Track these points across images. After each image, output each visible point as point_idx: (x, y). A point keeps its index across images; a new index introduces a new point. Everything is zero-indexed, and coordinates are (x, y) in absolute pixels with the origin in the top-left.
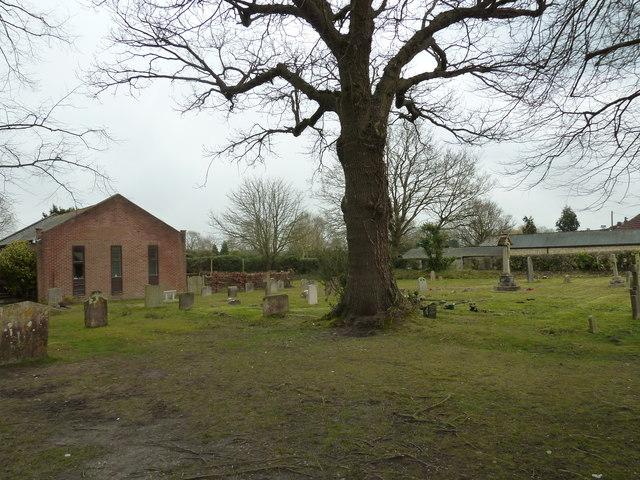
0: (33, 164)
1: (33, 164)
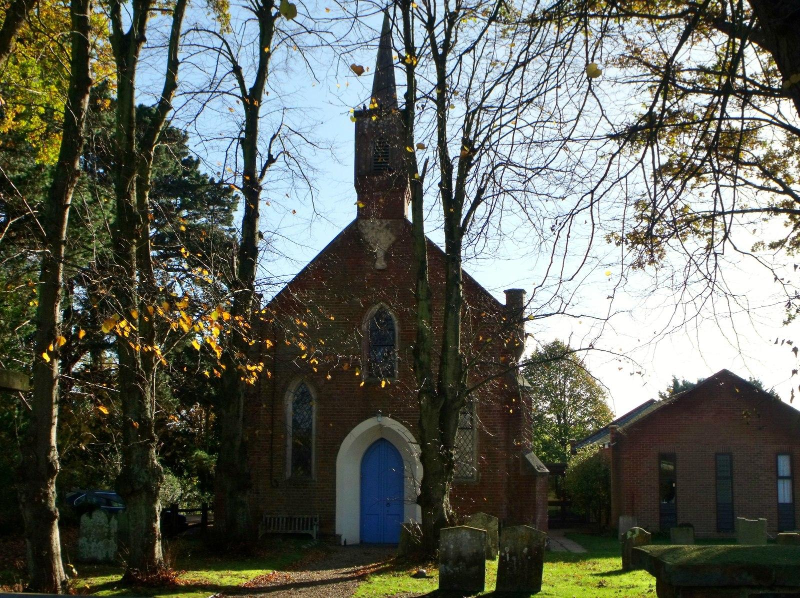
0: (603, 115)
1: (603, 115)
